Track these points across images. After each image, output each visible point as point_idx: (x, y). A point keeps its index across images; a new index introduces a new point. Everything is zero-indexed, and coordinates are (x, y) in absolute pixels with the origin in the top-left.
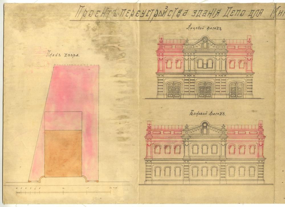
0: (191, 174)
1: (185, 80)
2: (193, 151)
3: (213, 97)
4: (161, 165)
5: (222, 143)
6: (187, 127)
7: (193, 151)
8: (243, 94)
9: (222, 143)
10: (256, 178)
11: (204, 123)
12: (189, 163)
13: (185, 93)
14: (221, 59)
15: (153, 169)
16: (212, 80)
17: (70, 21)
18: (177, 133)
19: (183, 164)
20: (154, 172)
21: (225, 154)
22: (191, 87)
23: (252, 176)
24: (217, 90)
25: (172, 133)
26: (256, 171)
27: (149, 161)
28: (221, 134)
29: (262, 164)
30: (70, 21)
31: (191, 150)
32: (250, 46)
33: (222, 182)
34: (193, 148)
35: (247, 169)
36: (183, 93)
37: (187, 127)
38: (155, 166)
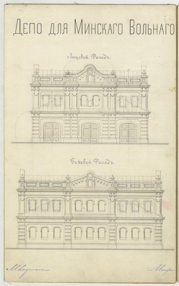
0: (28, 235)
1: (65, 120)
2: (29, 206)
3: (100, 141)
4: (48, 225)
5: (157, 199)
6: (68, 178)
7: (29, 206)
8: (59, 137)
9: (157, 199)
10: (106, 241)
11: (90, 173)
12: (25, 222)
13: (104, 137)
14: (109, 95)
15: (73, 230)
16: (97, 121)
17: (30, 33)
18: (134, 186)
19: (108, 224)
20: (28, 233)
21: (115, 212)
22: (111, 129)
23: (45, 238)
24: (104, 133)
25: (51, 185)
26: (107, 233)
27: (112, 221)
28: (109, 187)
29: (160, 225)
30: (30, 33)
31: (73, 206)
32: (111, 81)
33: (66, 246)
34: (29, 204)
35: (51, 230)
36: (102, 137)
37: (68, 178)
38: (30, 226)
